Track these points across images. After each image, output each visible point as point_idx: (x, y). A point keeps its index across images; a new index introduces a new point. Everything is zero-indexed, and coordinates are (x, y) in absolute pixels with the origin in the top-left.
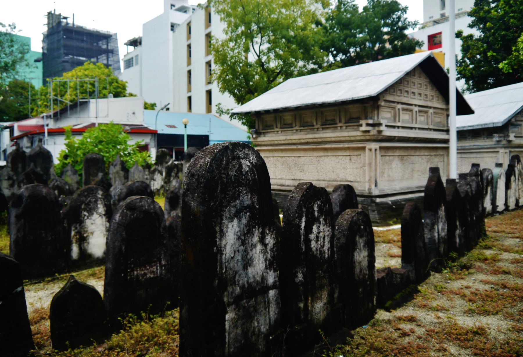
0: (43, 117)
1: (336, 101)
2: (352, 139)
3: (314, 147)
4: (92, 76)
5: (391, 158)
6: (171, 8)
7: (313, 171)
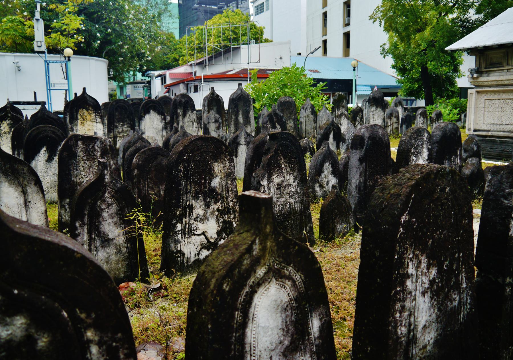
3: (502, 89)
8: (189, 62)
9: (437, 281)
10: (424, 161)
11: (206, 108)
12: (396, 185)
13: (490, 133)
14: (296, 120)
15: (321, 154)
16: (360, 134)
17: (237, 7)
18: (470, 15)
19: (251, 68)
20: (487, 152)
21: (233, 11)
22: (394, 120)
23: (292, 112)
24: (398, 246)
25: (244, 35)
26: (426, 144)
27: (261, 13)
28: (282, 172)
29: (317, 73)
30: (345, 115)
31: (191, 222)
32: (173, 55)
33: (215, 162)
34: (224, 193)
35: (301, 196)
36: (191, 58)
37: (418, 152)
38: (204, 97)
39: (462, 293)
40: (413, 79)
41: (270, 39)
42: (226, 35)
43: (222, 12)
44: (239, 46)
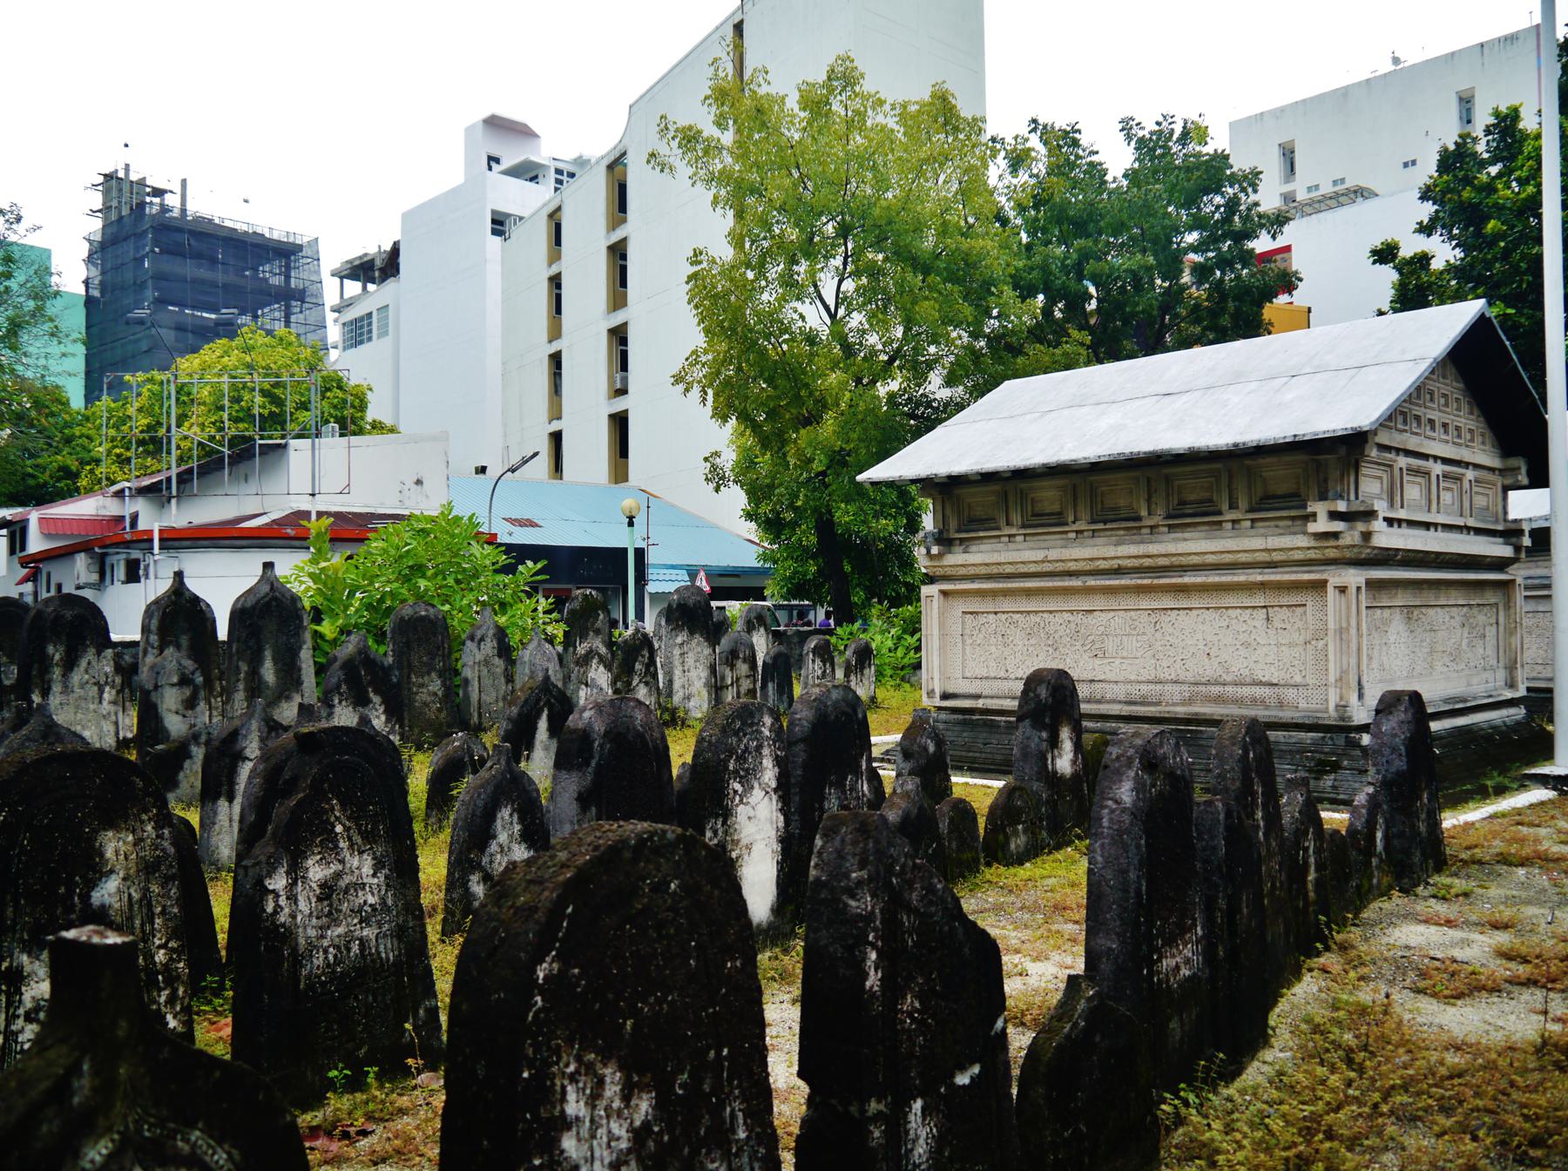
0: (120, 494)
1: (1236, 445)
2: (1277, 557)
4: (268, 368)
5: (1387, 612)
6: (490, 168)
7: (1139, 655)
8: (113, 483)
9: (656, 1129)
10: (767, 793)
11: (154, 638)
12: (530, 882)
13: (980, 704)
14: (450, 673)
15: (488, 782)
16: (580, 725)
17: (288, 323)
18: (930, 388)
19: (323, 508)
20: (977, 755)
21: (269, 333)
22: (743, 668)
23: (438, 649)
24: (530, 1045)
25: (304, 406)
26: (769, 746)
27: (361, 342)
28: (336, 847)
29: (530, 529)
30: (600, 656)
31: (14, 1028)
32: (59, 457)
33: (105, 830)
34: (137, 922)
35: (397, 916)
36: (121, 469)
37: (747, 770)
38: (152, 598)
39: (737, 1155)
40: (806, 549)
41: (388, 422)
42: (243, 403)
43: (232, 335)
44: (283, 442)
